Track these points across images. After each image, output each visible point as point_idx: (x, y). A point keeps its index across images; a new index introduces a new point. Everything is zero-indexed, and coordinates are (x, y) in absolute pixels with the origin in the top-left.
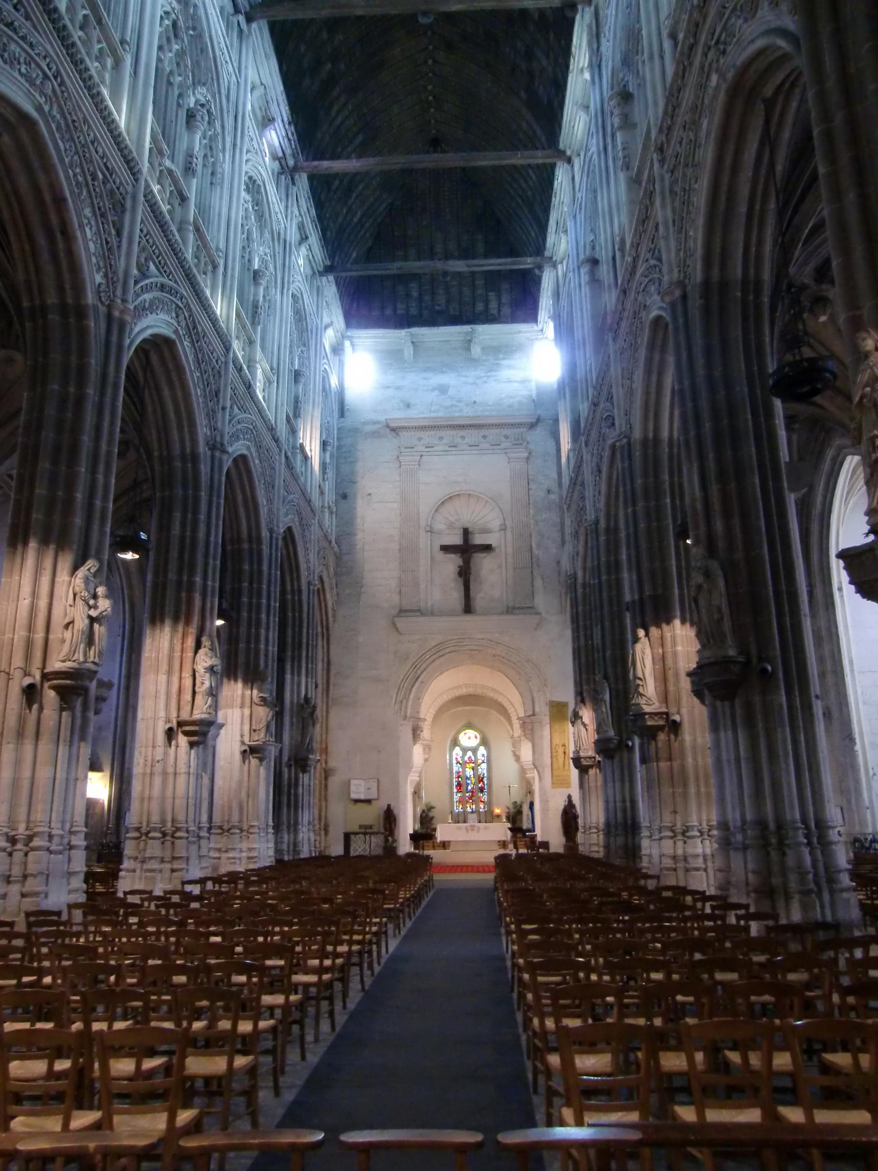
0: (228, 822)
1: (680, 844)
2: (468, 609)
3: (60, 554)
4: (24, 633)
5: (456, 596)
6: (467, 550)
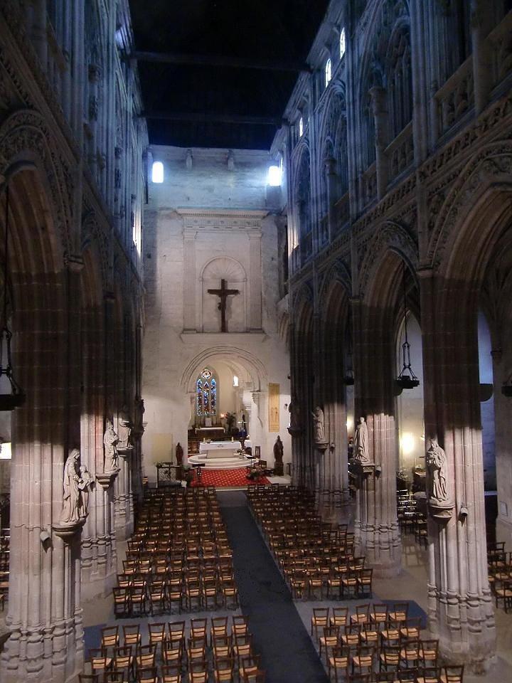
1: (377, 534)
2: (224, 329)
3: (54, 446)
5: (215, 320)
6: (224, 292)
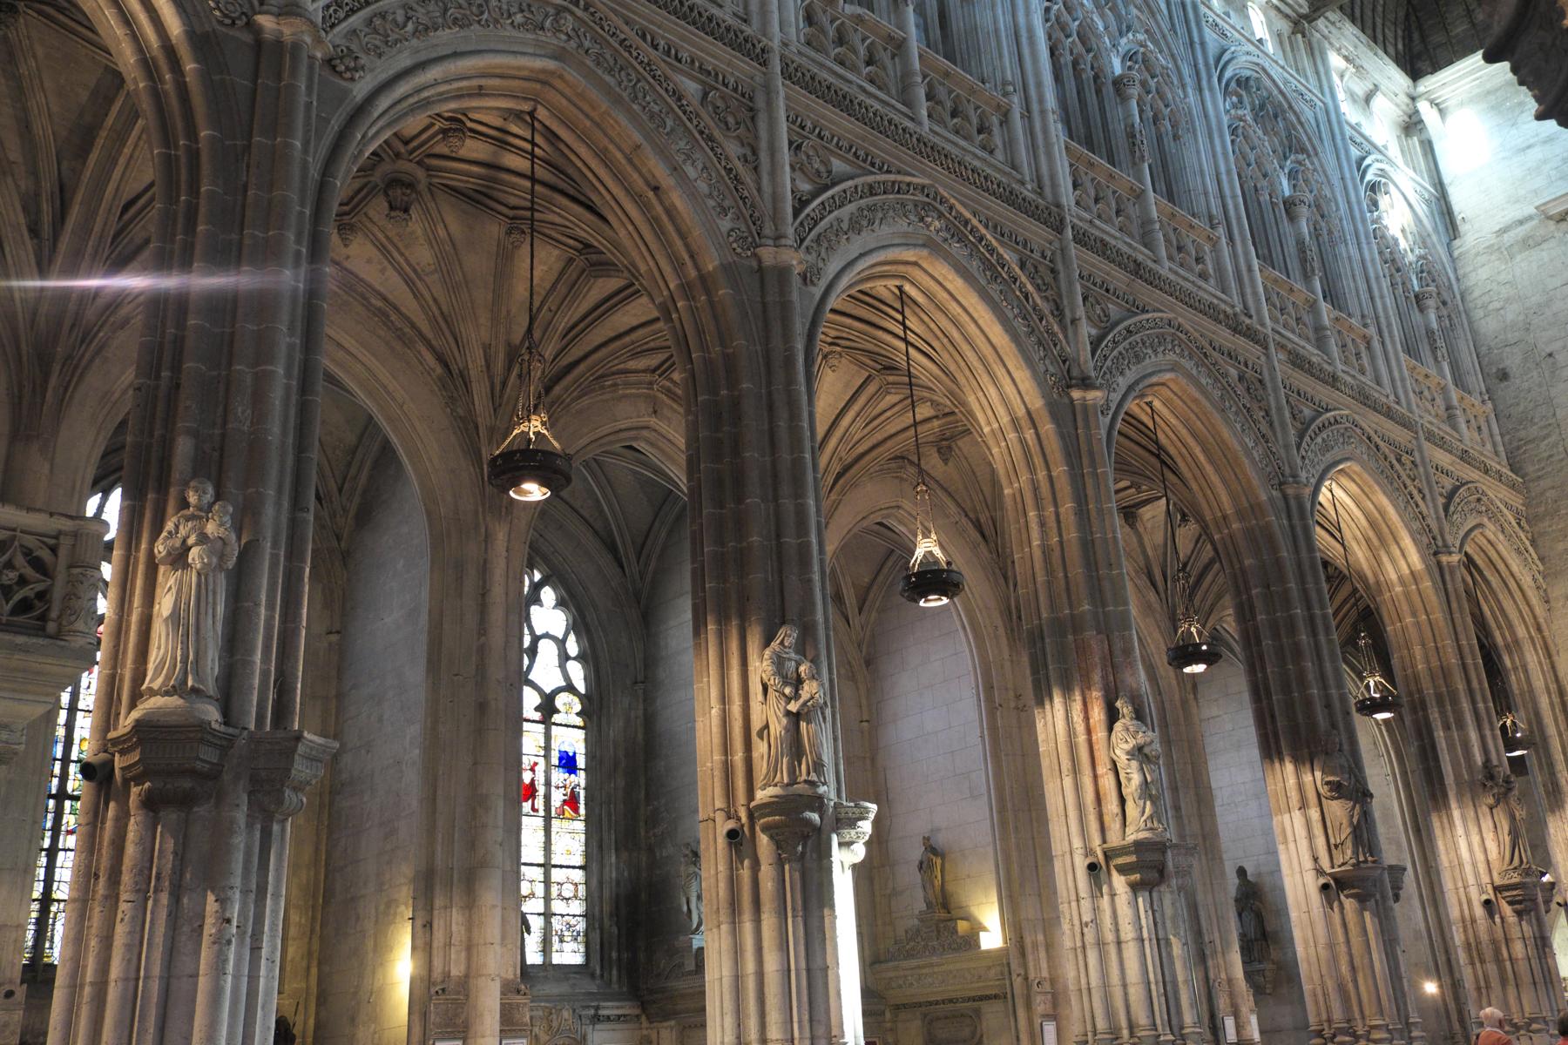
0: (1329, 1021)
4: (718, 757)
